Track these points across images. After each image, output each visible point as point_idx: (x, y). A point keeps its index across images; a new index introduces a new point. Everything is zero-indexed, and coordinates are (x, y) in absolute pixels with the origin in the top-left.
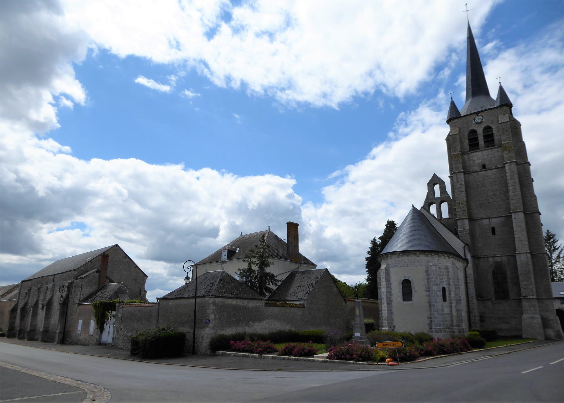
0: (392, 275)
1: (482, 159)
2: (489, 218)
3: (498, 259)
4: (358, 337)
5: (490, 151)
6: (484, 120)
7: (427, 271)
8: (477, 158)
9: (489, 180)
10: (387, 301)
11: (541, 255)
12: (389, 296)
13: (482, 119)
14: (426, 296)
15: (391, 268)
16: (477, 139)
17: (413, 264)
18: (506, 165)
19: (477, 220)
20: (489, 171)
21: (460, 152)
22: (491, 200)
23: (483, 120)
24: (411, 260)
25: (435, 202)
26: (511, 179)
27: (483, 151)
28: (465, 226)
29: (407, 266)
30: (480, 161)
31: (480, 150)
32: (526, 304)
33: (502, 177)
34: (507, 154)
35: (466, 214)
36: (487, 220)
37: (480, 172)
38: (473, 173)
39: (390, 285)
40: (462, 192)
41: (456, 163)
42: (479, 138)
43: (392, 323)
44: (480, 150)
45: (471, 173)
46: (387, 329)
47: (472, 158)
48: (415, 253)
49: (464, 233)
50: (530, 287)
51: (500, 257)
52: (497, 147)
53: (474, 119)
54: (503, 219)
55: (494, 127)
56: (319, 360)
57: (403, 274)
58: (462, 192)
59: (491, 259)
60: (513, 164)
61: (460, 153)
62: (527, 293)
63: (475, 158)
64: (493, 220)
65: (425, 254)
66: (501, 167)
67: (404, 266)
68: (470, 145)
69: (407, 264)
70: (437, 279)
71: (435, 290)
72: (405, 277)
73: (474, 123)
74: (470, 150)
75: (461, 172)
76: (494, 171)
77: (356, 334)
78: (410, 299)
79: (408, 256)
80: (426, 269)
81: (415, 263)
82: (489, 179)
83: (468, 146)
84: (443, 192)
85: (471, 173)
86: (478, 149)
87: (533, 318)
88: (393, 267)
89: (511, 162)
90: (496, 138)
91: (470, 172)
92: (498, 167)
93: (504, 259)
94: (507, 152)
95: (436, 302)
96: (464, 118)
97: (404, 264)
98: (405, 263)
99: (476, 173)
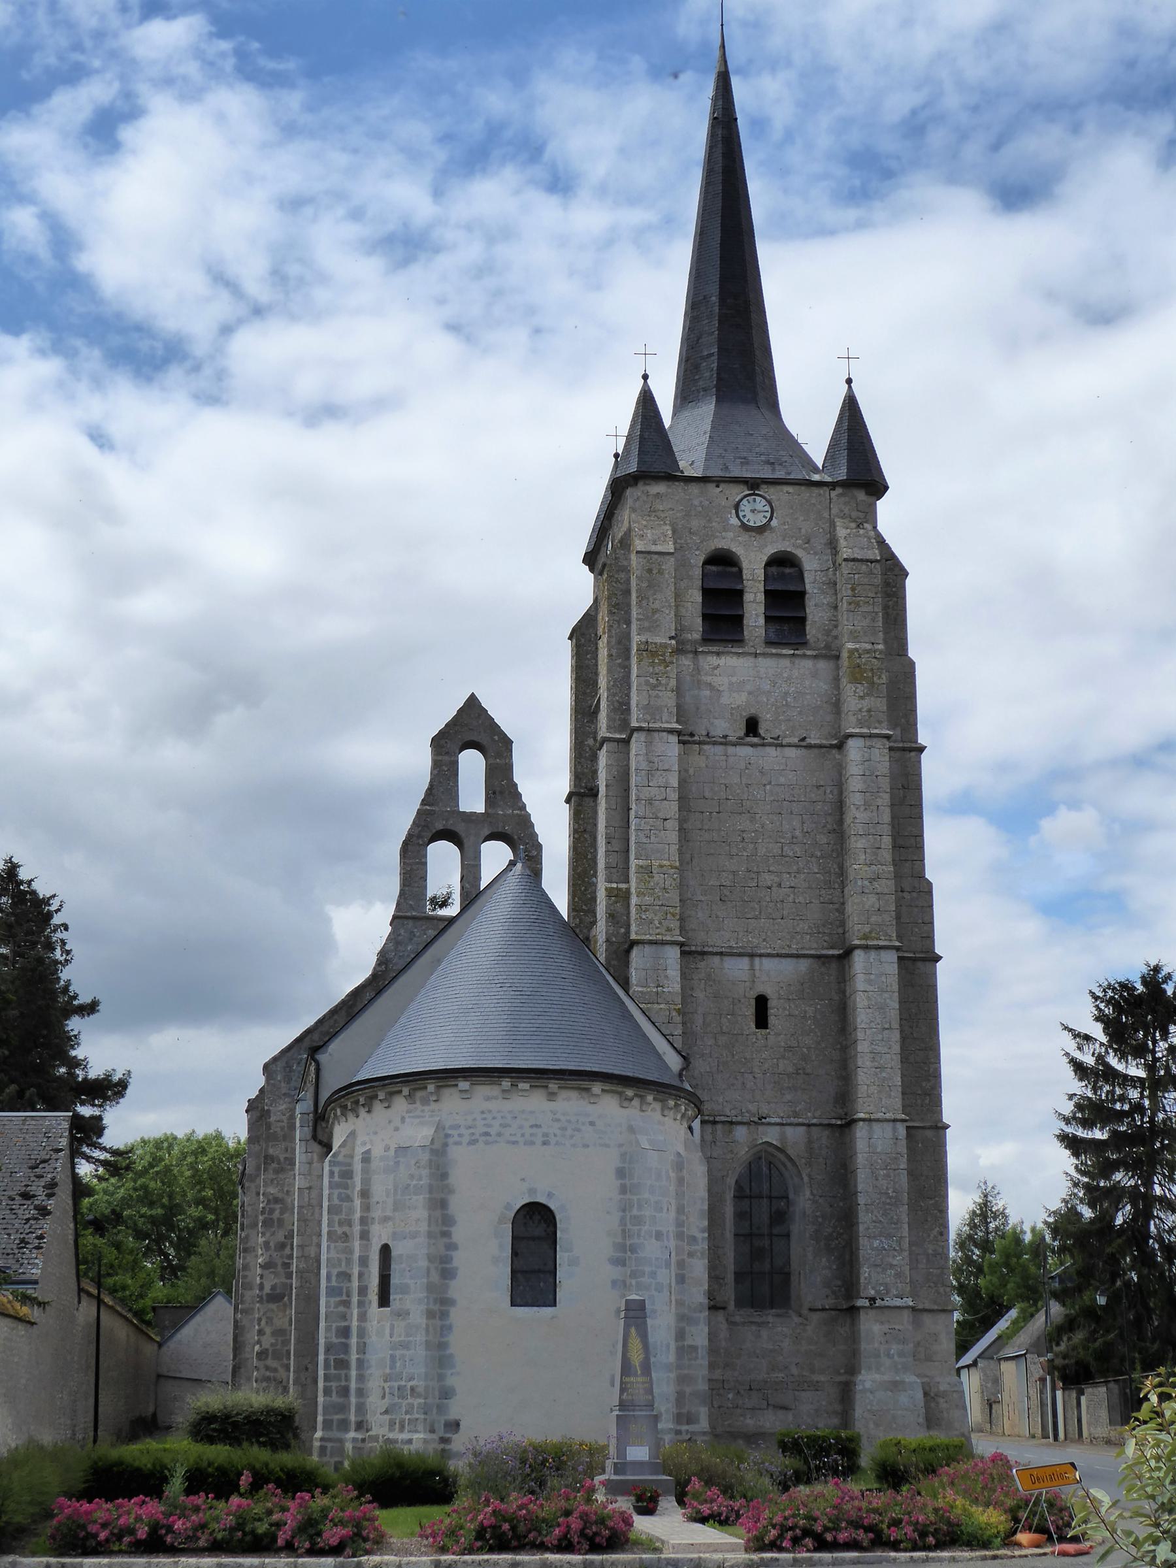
0: (459, 1177)
1: (750, 693)
2: (752, 956)
3: (771, 1136)
4: (641, 1464)
5: (786, 662)
6: (774, 523)
7: (621, 1173)
8: (731, 684)
9: (768, 787)
11: (929, 1133)
12: (435, 1277)
13: (768, 515)
14: (614, 1283)
15: (457, 1143)
16: (737, 596)
17: (572, 1137)
18: (851, 743)
19: (703, 953)
20: (771, 751)
21: (671, 638)
22: (768, 879)
23: (771, 518)
24: (564, 1114)
25: (462, 834)
26: (867, 805)
27: (756, 655)
28: (666, 977)
29: (544, 1143)
30: (741, 699)
31: (746, 649)
32: (877, 1328)
33: (818, 787)
34: (862, 698)
35: (675, 924)
36: (745, 961)
37: (734, 745)
38: (708, 743)
40: (666, 820)
41: (654, 687)
42: (748, 597)
43: (441, 1409)
44: (746, 649)
45: (700, 743)
46: (422, 1436)
47: (709, 679)
48: (585, 1084)
49: (662, 1006)
50: (895, 1262)
51: (778, 1128)
52: (815, 657)
53: (737, 507)
54: (804, 965)
55: (811, 565)
56: (725, 1560)
57: (523, 1180)
58: (666, 820)
59: (741, 1133)
60: (878, 743)
61: (673, 642)
62: (881, 1284)
63: (721, 681)
64: (768, 963)
65: (620, 1094)
66: (821, 746)
67: (533, 1143)
68: (705, 617)
69: (546, 1135)
72: (532, 1191)
73: (734, 521)
74: (706, 640)
75: (671, 731)
76: (792, 753)
78: (548, 1298)
79: (552, 1096)
81: (579, 1130)
82: (770, 783)
83: (699, 620)
84: (501, 793)
85: (700, 743)
86: (740, 641)
87: (895, 1386)
88: (473, 1142)
89: (871, 736)
90: (816, 613)
91: (696, 738)
92: (808, 741)
93: (795, 1137)
94: (861, 690)
96: (694, 489)
97: (534, 1130)
98: (537, 1126)
99: (719, 749)
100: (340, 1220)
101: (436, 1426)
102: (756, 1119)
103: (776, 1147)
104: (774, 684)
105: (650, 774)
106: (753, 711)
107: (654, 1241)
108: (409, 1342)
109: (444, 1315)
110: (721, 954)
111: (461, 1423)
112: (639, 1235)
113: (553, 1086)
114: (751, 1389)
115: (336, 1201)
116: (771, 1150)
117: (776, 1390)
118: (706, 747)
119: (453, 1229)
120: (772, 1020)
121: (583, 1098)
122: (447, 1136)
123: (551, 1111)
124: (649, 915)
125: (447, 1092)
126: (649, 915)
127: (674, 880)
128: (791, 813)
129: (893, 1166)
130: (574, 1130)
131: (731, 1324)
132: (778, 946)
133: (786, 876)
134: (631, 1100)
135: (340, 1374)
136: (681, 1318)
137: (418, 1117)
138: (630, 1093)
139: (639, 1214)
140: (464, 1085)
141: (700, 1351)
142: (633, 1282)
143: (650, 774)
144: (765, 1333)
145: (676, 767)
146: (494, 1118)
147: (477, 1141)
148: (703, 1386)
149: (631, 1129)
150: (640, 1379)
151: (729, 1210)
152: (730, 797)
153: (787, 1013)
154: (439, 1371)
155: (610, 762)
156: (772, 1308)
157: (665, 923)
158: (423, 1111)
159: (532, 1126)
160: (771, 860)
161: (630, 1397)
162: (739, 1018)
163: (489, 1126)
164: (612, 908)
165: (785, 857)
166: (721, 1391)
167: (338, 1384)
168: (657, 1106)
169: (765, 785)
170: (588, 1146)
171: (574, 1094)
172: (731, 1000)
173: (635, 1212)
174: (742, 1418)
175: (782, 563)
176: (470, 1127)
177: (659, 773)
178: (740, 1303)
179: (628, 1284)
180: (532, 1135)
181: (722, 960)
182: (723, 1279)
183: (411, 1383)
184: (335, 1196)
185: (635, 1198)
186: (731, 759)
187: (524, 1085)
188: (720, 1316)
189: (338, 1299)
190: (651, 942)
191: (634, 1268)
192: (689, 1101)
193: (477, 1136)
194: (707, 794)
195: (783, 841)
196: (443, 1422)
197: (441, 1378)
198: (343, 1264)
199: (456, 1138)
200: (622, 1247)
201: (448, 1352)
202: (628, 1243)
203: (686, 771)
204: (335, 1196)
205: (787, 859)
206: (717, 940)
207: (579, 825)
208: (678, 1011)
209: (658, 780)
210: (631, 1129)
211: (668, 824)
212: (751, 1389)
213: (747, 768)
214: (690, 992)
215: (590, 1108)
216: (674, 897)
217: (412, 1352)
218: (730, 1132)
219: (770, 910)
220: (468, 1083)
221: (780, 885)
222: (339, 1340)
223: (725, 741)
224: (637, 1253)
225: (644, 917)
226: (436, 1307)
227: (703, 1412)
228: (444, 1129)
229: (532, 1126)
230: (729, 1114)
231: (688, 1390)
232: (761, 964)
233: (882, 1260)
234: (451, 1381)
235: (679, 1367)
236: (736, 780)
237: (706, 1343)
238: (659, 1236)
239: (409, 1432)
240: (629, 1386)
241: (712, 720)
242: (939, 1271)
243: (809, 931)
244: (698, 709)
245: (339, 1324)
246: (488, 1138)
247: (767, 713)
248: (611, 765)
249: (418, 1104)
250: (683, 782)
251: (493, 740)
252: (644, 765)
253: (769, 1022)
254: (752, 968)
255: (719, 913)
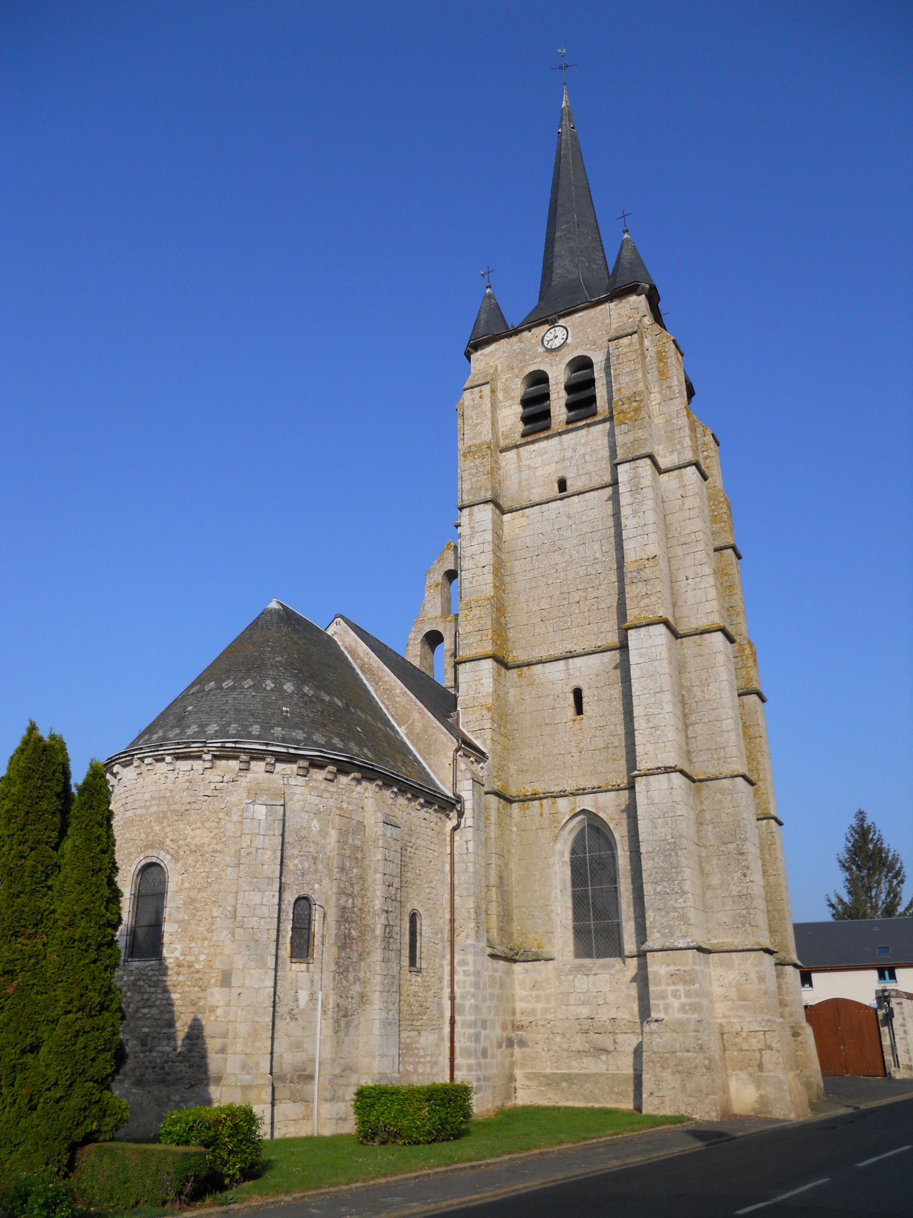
5: (583, 432)
23: (567, 338)
40: (483, 567)
50: (677, 905)
58: (483, 567)
104: (575, 450)
106: (560, 474)
129: (670, 814)
132: (589, 645)
152: (546, 542)
175: (582, 364)
195: (587, 564)
205: (591, 577)
233: (665, 904)
242: (745, 912)
243: (611, 629)
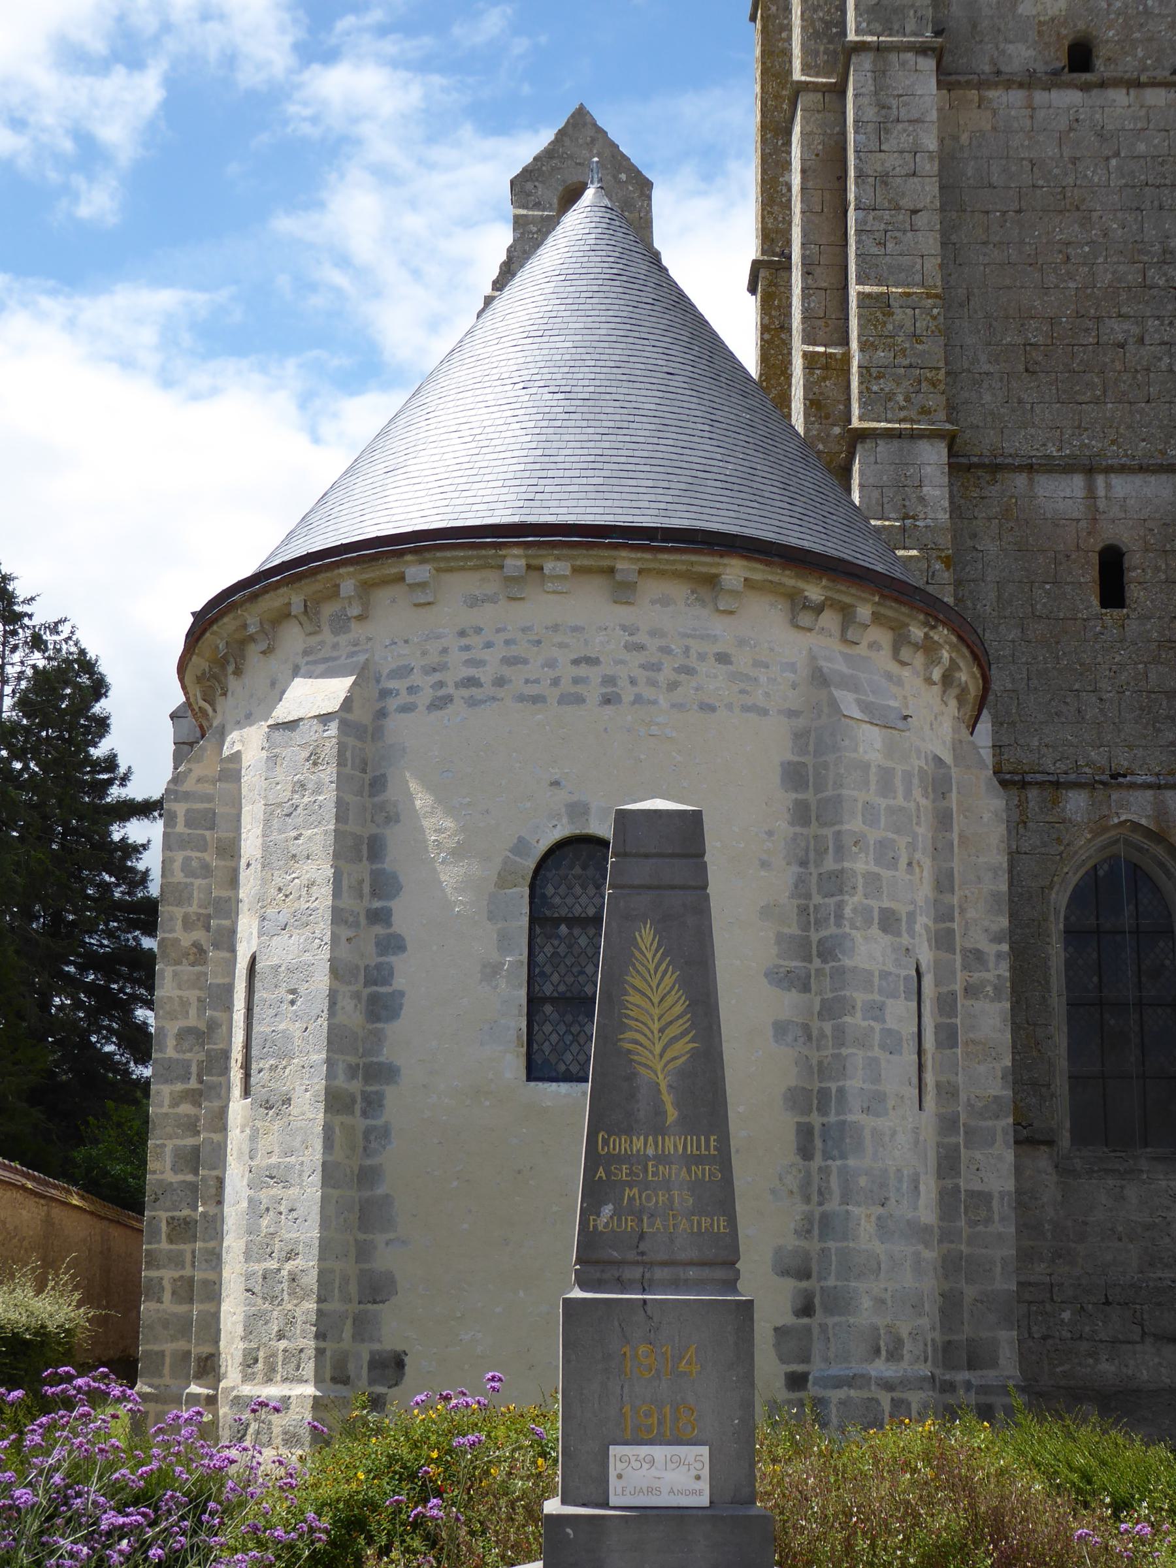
2: (1090, 471)
7: (795, 776)
9: (1114, 162)
10: (330, 1076)
15: (407, 709)
17: (673, 686)
20: (1119, 97)
22: (1117, 329)
24: (653, 633)
28: (921, 499)
29: (607, 701)
35: (934, 401)
36: (1078, 482)
38: (996, 85)
39: (374, 894)
40: (915, 212)
43: (363, 1326)
51: (1149, 793)
57: (556, 784)
58: (915, 212)
59: (1076, 803)
64: (1122, 486)
67: (579, 700)
69: (610, 680)
70: (893, 863)
71: (870, 973)
72: (578, 810)
77: (614, 1450)
79: (623, 592)
80: (790, 757)
81: (689, 671)
82: (1117, 154)
88: (440, 703)
95: (875, 1103)
97: (583, 670)
99: (1016, 97)
100: (186, 918)
101: (351, 1367)
102: (1105, 778)
103: (1147, 832)
105: (882, 129)
106: (1081, 25)
107: (875, 930)
108: (289, 1168)
109: (373, 1104)
110: (1030, 468)
111: (407, 1360)
112: (839, 916)
113: (626, 563)
114: (1107, 1303)
115: (179, 877)
116: (1137, 838)
117: (1159, 1304)
118: (992, 94)
119: (395, 905)
120: (1133, 592)
121: (701, 601)
122: (385, 694)
123: (624, 628)
124: (887, 385)
125: (383, 596)
126: (887, 385)
127: (934, 318)
128: (1161, 208)
130: (679, 670)
131: (1063, 1170)
133: (1152, 324)
134: (819, 609)
135: (181, 1253)
136: (948, 1124)
137: (325, 660)
138: (814, 592)
139: (838, 867)
140: (416, 571)
141: (995, 1203)
142: (828, 1027)
143: (882, 129)
144: (1132, 1192)
145: (934, 115)
146: (489, 645)
147: (448, 699)
148: (1004, 1284)
149: (820, 678)
150: (672, 1144)
151: (1056, 952)
152: (1041, 183)
153: (1163, 577)
154: (361, 1237)
155: (808, 129)
156: (1146, 1145)
157: (918, 399)
158: (335, 646)
159: (576, 662)
160: (1124, 296)
161: (629, 1224)
162: (1068, 588)
163: (479, 663)
164: (816, 389)
165: (1151, 288)
166: (1048, 1308)
167: (176, 1275)
168: (883, 636)
169: (1108, 159)
170: (713, 709)
171: (679, 591)
172: (1051, 554)
173: (830, 864)
174: (1091, 1361)
176: (434, 670)
177: (900, 126)
178: (1080, 1137)
179: (815, 1033)
180: (576, 681)
181: (1031, 480)
182: (1048, 1086)
183: (289, 1266)
184: (177, 865)
185: (828, 832)
186: (1041, 114)
187: (552, 566)
188: (1042, 1160)
189: (179, 1087)
190: (889, 434)
191: (830, 995)
192: (960, 637)
193: (451, 690)
194: (995, 179)
196: (366, 1357)
197: (363, 1252)
198: (193, 1012)
199: (404, 698)
200: (802, 948)
201: (380, 1191)
202: (815, 937)
203: (956, 138)
204: (177, 865)
205: (1154, 292)
206: (1019, 444)
207: (771, 317)
208: (948, 562)
209: (899, 138)
210: (820, 678)
211: (921, 220)
212: (1107, 1303)
213: (1071, 129)
214: (970, 543)
215: (719, 626)
216: (933, 349)
217: (294, 1191)
218: (1055, 802)
219: (1123, 387)
220: (428, 567)
221: (1141, 341)
222: (180, 1177)
223: (1028, 81)
224: (836, 959)
225: (875, 388)
226: (355, 1086)
227: (1006, 1342)
228: (378, 681)
229: (576, 662)
230: (1052, 769)
231: (970, 1292)
232: (1108, 486)
234: (386, 1259)
235: (947, 1236)
236: (1051, 151)
237: (1010, 1185)
238: (889, 922)
239: (285, 1380)
240: (623, 1173)
241: (1002, 46)
244: (974, 26)
245: (179, 1142)
246: (474, 691)
247: (1109, 28)
248: (811, 133)
249: (327, 635)
250: (948, 159)
251: (619, 182)
252: (870, 113)
253: (1127, 595)
254: (1091, 489)
255: (1024, 396)
